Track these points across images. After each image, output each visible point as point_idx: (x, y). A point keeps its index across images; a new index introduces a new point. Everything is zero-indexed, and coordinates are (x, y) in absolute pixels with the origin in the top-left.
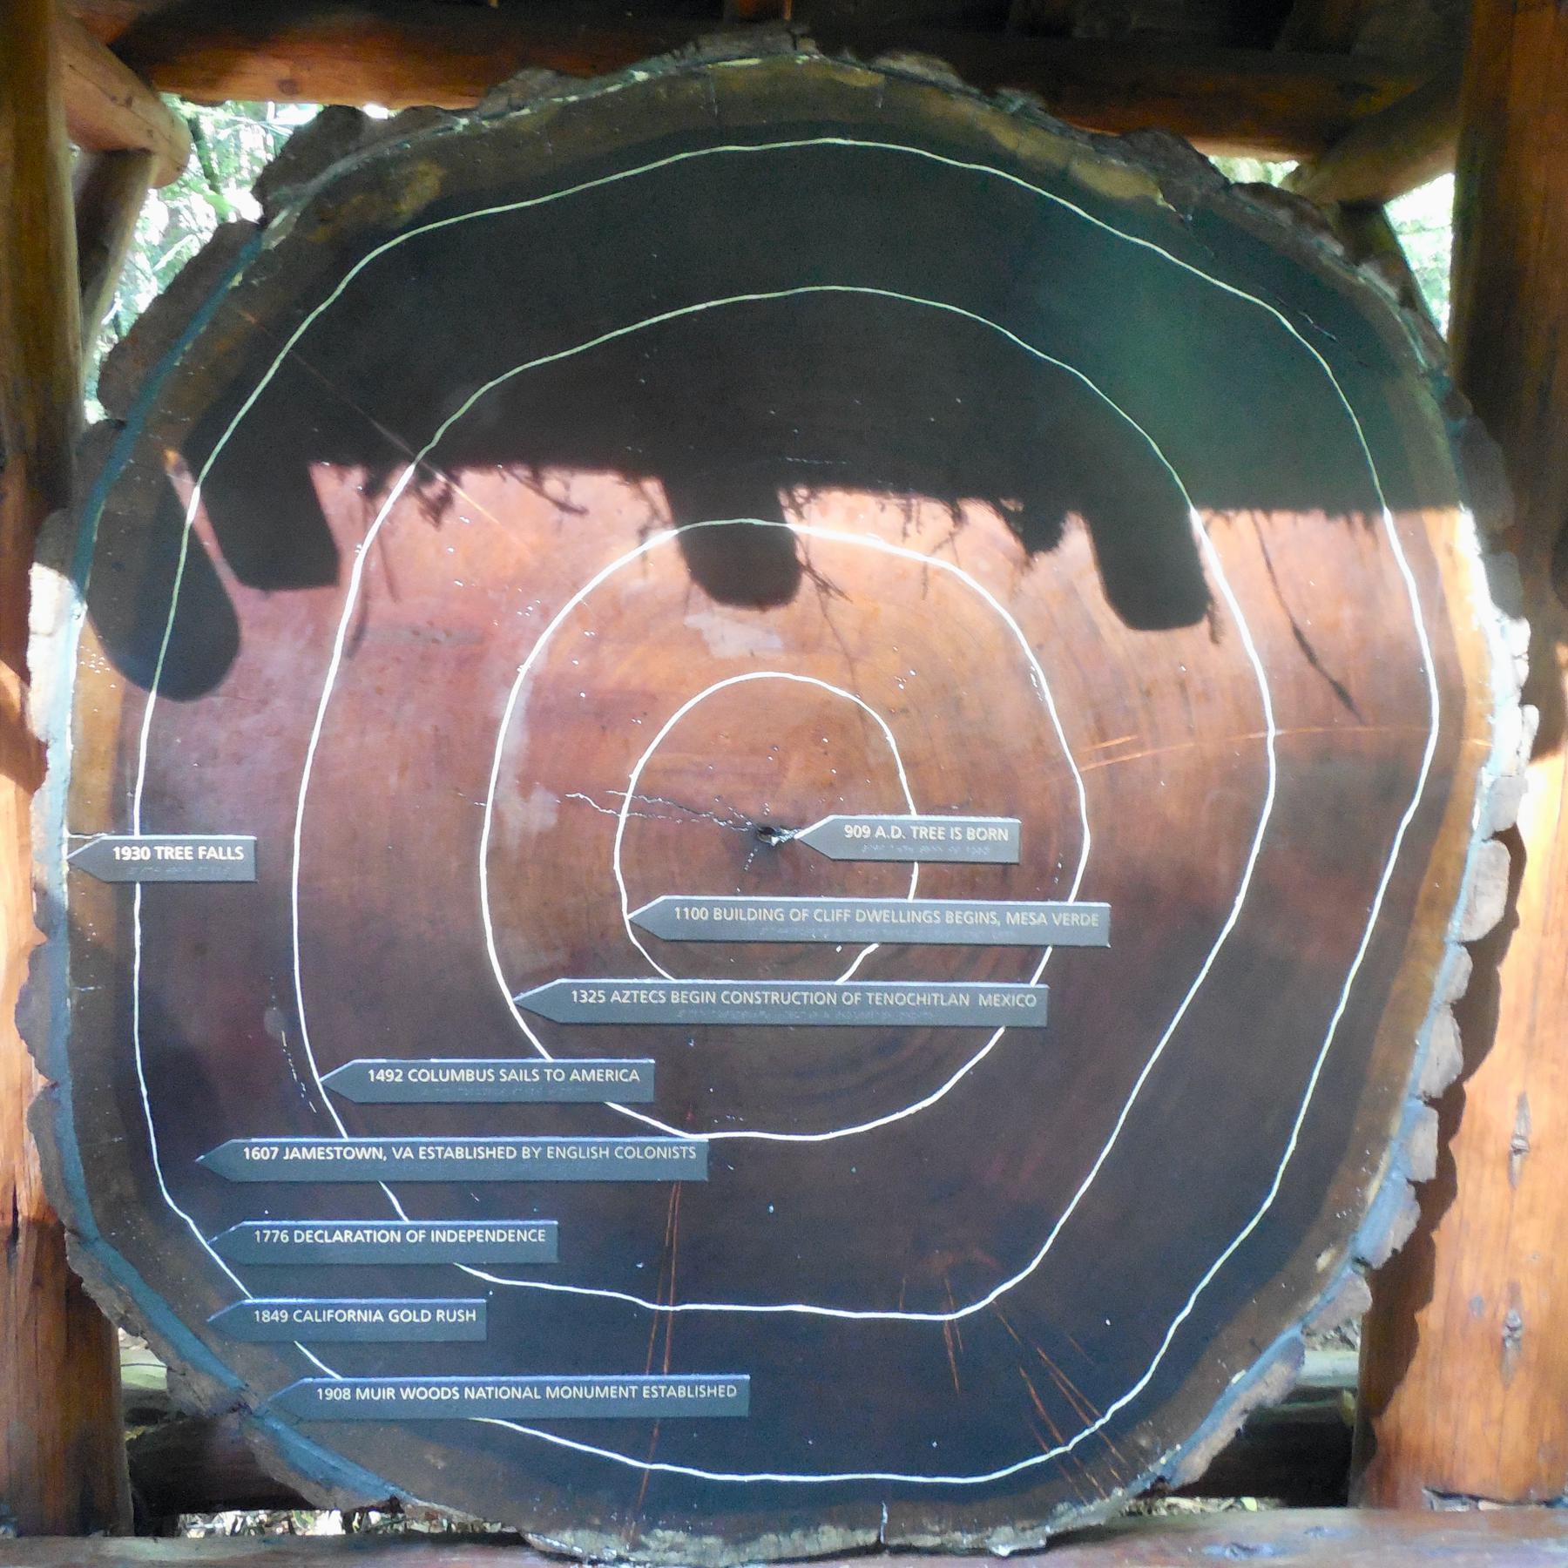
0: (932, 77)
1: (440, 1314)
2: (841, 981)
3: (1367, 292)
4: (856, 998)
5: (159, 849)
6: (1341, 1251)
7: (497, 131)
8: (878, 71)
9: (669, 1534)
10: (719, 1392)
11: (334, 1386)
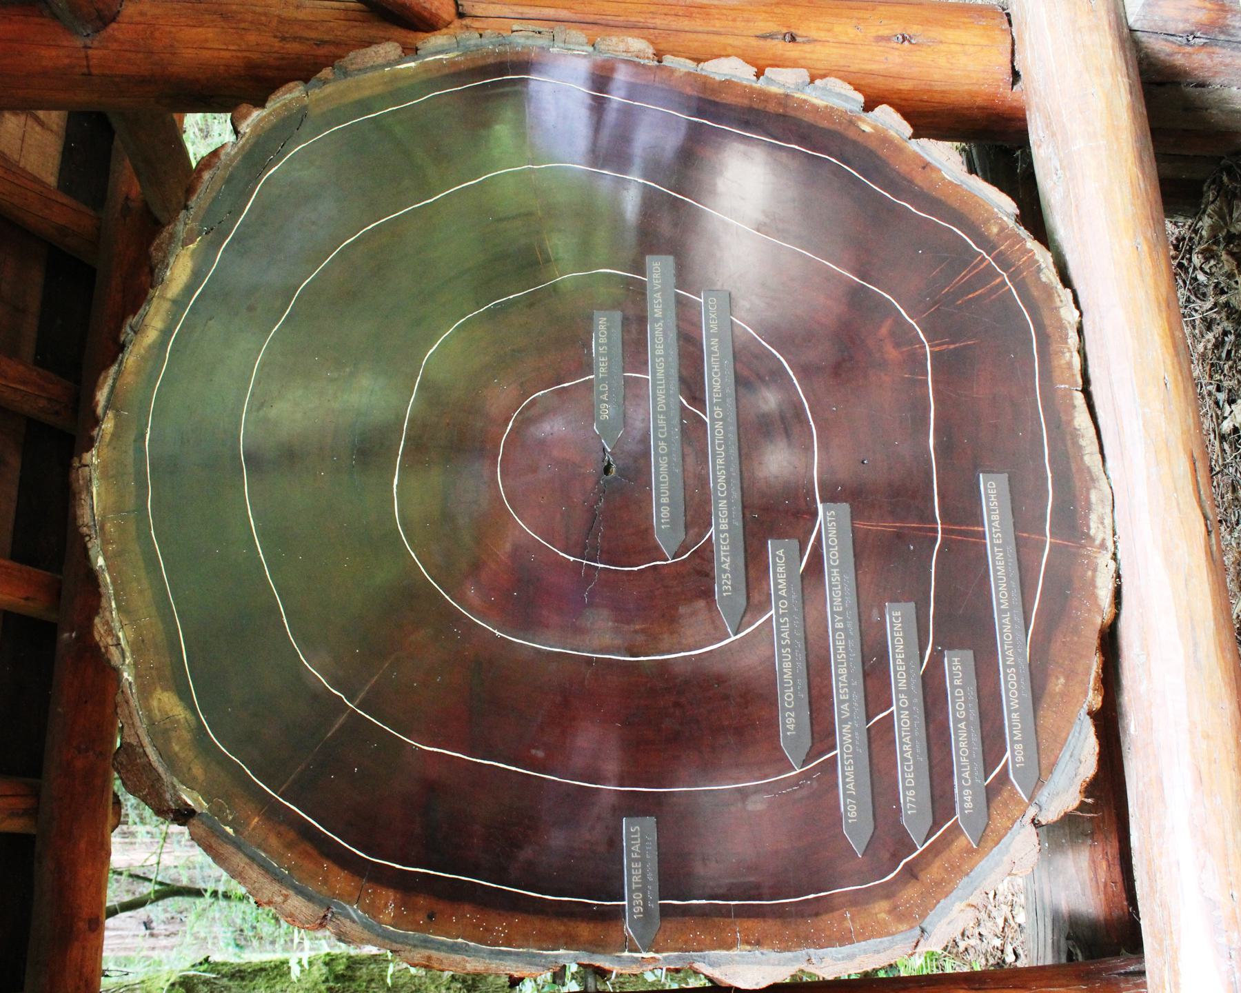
0: (110, 382)
1: (957, 682)
2: (707, 420)
3: (255, 126)
4: (717, 409)
5: (634, 886)
6: (860, 119)
7: (133, 653)
8: (105, 413)
9: (1093, 525)
10: (993, 492)
11: (1013, 756)
